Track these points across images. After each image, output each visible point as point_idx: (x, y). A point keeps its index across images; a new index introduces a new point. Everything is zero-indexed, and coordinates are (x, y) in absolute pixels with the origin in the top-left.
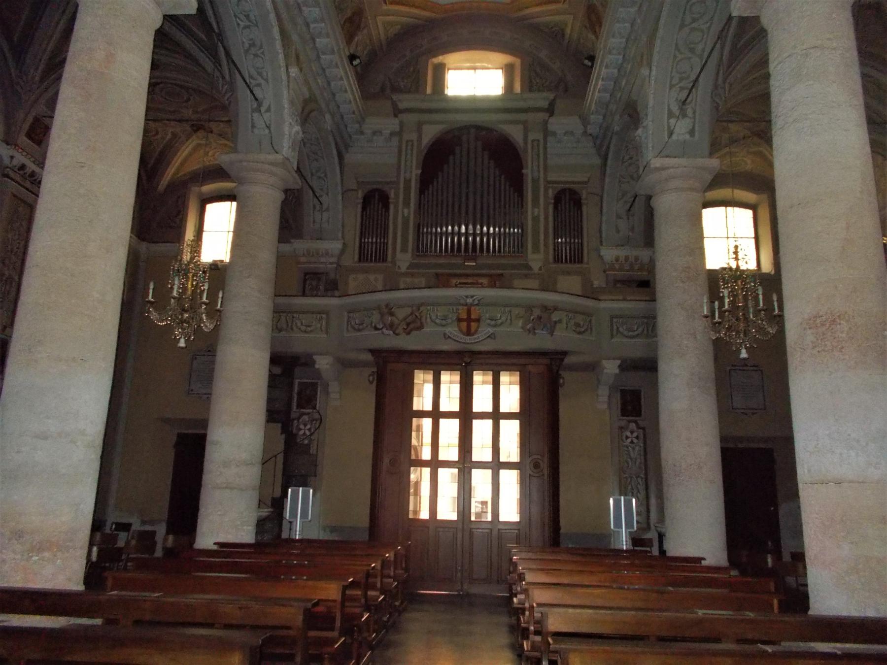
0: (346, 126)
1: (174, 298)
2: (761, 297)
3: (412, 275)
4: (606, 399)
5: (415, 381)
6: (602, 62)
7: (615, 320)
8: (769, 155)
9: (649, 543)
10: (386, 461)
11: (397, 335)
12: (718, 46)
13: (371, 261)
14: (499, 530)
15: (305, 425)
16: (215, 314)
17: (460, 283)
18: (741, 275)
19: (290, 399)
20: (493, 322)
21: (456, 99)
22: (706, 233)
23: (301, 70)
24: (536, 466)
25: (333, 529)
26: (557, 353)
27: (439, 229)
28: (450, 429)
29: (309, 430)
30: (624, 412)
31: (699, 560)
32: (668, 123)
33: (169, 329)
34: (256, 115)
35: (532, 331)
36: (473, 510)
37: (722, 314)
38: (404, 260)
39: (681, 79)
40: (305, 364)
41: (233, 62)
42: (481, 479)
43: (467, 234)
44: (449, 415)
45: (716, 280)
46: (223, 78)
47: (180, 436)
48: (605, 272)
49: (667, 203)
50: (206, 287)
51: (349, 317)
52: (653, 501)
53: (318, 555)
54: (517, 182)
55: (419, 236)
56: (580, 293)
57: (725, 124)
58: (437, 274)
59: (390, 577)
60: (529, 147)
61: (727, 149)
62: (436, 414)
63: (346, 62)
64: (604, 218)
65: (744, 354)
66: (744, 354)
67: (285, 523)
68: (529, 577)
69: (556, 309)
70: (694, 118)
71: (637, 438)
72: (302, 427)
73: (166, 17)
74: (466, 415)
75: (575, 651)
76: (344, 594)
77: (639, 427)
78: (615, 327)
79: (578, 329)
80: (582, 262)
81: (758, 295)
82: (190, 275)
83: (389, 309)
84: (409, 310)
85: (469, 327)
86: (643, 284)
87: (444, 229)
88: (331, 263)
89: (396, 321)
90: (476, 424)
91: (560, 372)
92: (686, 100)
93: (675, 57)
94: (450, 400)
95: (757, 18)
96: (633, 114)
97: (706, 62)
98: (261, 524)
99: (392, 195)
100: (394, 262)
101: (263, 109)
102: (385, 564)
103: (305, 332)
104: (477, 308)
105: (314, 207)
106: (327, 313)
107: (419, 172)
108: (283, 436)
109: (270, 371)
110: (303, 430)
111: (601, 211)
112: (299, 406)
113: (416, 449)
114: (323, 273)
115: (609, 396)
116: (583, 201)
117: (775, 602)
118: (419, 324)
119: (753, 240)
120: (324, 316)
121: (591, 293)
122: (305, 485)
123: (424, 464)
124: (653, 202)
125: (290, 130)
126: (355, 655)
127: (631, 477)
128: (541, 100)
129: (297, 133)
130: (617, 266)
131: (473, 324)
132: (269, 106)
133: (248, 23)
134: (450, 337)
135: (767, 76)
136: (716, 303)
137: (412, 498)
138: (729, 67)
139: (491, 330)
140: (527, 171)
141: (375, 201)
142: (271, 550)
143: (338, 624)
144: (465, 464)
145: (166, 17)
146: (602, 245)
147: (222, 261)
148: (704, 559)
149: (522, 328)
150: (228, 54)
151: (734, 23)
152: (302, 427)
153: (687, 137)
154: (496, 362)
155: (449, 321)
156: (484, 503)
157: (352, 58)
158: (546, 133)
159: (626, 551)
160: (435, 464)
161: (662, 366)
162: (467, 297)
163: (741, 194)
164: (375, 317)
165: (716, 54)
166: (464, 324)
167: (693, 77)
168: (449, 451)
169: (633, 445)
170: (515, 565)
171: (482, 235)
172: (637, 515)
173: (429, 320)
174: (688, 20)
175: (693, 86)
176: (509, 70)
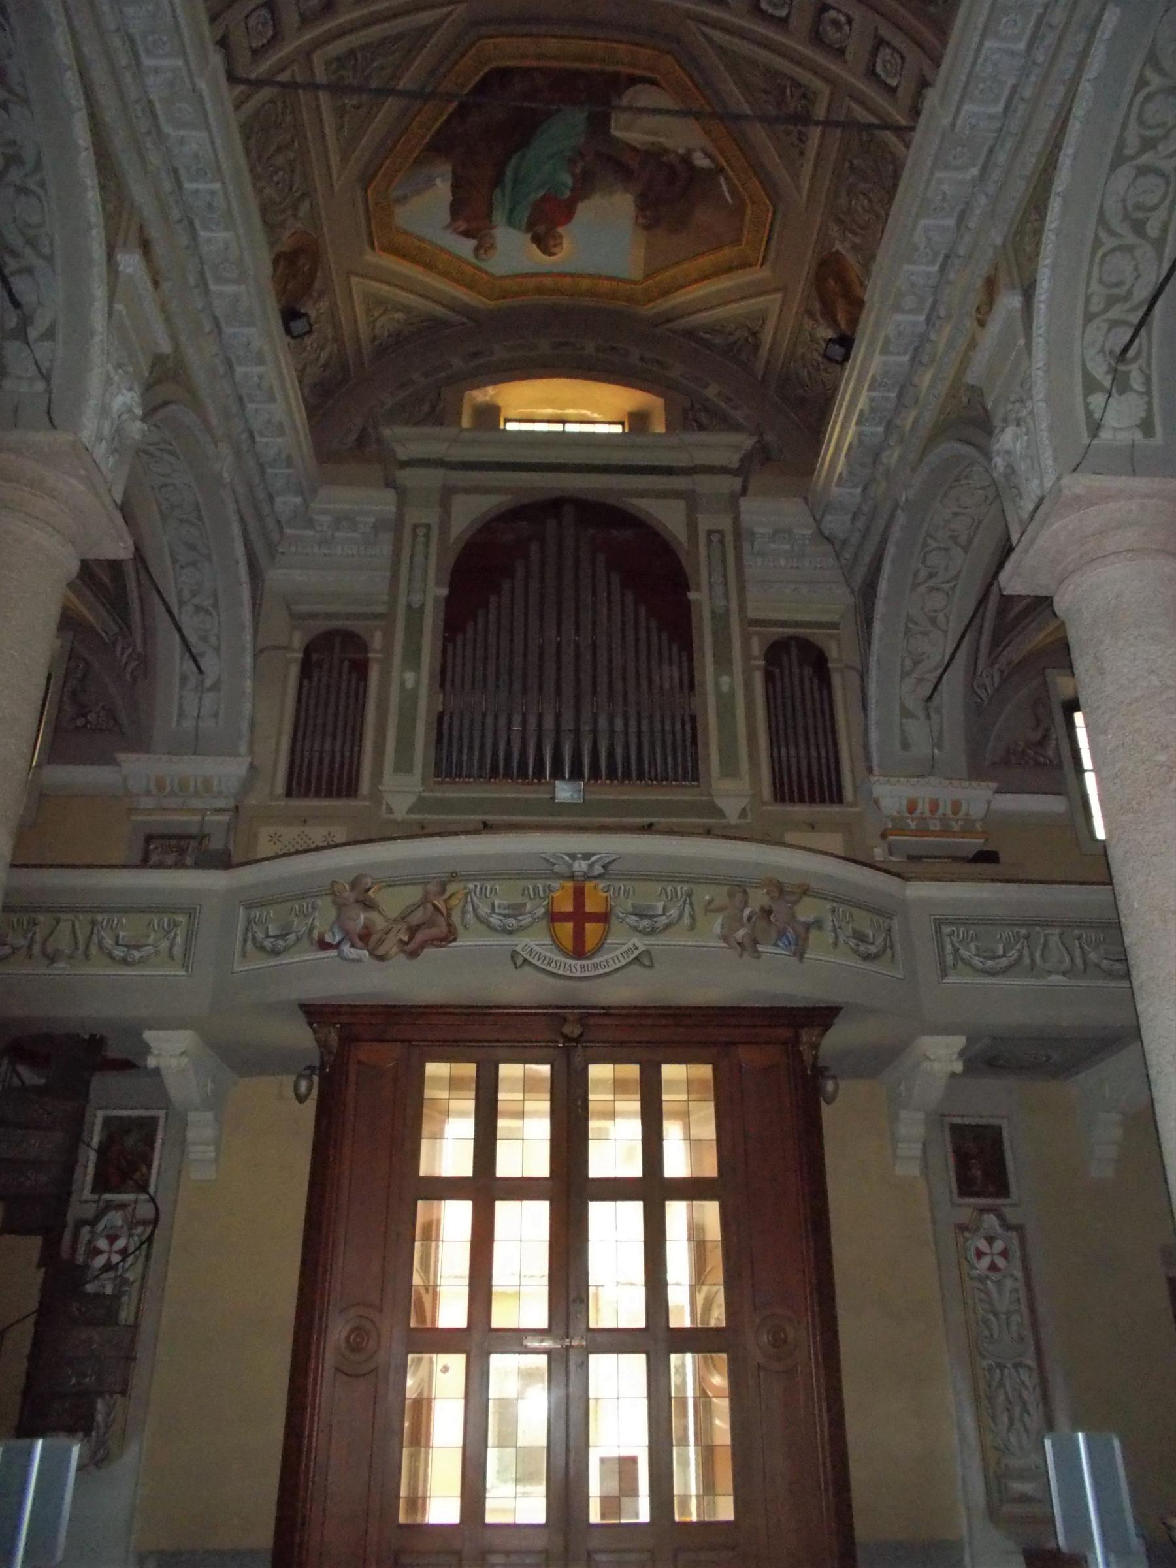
0: (271, 498)
4: (916, 1150)
10: (337, 1331)
11: (381, 958)
15: (112, 1239)
20: (645, 922)
28: (524, 1227)
30: (966, 1187)
32: (1087, 405)
35: (749, 947)
39: (1111, 301)
40: (126, 1065)
62: (485, 1188)
69: (805, 891)
70: (1148, 393)
71: (1004, 1254)
72: (102, 1244)
77: (1006, 1226)
78: (949, 948)
80: (840, 801)
89: (380, 923)
90: (600, 1213)
93: (1097, 242)
94: (526, 1149)
99: (377, 641)
100: (376, 797)
101: (33, 334)
103: (125, 962)
104: (602, 885)
105: (184, 679)
106: (191, 913)
107: (444, 592)
112: (102, 1183)
114: (191, 837)
118: (441, 929)
120: (182, 919)
123: (448, 1341)
127: (1002, 1367)
130: (913, 825)
131: (589, 926)
139: (641, 943)
141: (333, 664)
149: (725, 938)
152: (102, 1244)
153: (1138, 435)
154: (651, 1035)
155: (527, 920)
156: (627, 1464)
160: (480, 1340)
162: (573, 856)
164: (323, 919)
167: (1142, 293)
168: (523, 1299)
169: (995, 1276)
173: (470, 916)
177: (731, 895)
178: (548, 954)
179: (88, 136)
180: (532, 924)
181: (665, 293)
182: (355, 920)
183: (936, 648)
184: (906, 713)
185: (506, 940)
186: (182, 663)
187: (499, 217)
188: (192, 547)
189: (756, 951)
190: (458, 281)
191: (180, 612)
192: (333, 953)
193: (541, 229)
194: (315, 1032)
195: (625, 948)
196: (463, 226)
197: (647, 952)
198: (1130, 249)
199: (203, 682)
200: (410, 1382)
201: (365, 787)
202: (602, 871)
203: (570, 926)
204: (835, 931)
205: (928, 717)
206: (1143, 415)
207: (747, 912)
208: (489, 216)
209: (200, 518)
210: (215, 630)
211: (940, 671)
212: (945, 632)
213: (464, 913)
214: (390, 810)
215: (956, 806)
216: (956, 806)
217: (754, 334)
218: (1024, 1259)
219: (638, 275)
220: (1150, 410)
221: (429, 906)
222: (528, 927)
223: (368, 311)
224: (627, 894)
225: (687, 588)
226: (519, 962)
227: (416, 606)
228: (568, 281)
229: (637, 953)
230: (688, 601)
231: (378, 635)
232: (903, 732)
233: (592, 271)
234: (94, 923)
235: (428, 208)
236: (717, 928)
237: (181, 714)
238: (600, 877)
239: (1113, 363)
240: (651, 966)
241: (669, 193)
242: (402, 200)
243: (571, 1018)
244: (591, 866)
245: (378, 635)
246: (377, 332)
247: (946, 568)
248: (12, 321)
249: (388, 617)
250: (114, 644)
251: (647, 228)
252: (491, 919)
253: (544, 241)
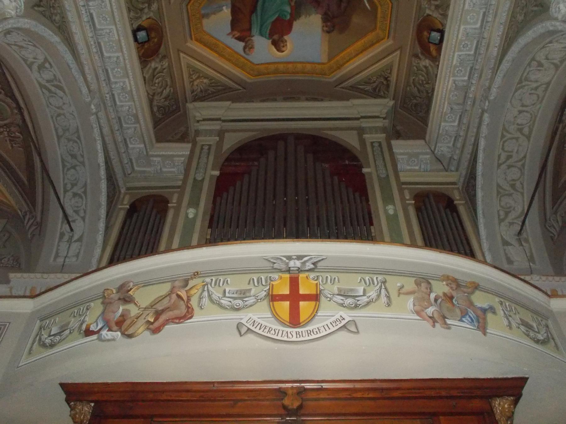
11: (130, 336)
20: (349, 301)
84: (165, 289)
89: (133, 310)
104: (312, 275)
105: (62, 235)
118: (183, 310)
139: (347, 315)
149: (418, 313)
155: (251, 300)
162: (289, 258)
164: (93, 317)
177: (418, 284)
178: (269, 325)
180: (255, 303)
181: (339, 67)
182: (114, 312)
183: (519, 204)
184: (506, 243)
186: (62, 226)
187: (255, 30)
188: (74, 156)
189: (445, 323)
190: (236, 65)
191: (64, 197)
192: (95, 337)
193: (276, 37)
194: (72, 409)
195: (334, 319)
196: (238, 34)
199: (72, 237)
202: (312, 266)
203: (287, 304)
207: (433, 296)
208: (250, 29)
209: (79, 138)
210: (84, 206)
211: (522, 218)
212: (522, 194)
213: (200, 298)
217: (386, 79)
219: (325, 60)
221: (174, 296)
222: (251, 306)
223: (190, 75)
224: (333, 281)
225: (361, 167)
226: (244, 330)
227: (200, 179)
228: (290, 66)
229: (344, 322)
230: (363, 175)
231: (176, 196)
232: (506, 254)
233: (301, 60)
237: (57, 256)
238: (310, 270)
240: (358, 332)
242: (206, 16)
243: (290, 392)
244: (304, 263)
245: (176, 196)
246: (195, 88)
247: (517, 152)
249: (182, 188)
250: (24, 217)
251: (328, 32)
252: (222, 301)
253: (278, 44)
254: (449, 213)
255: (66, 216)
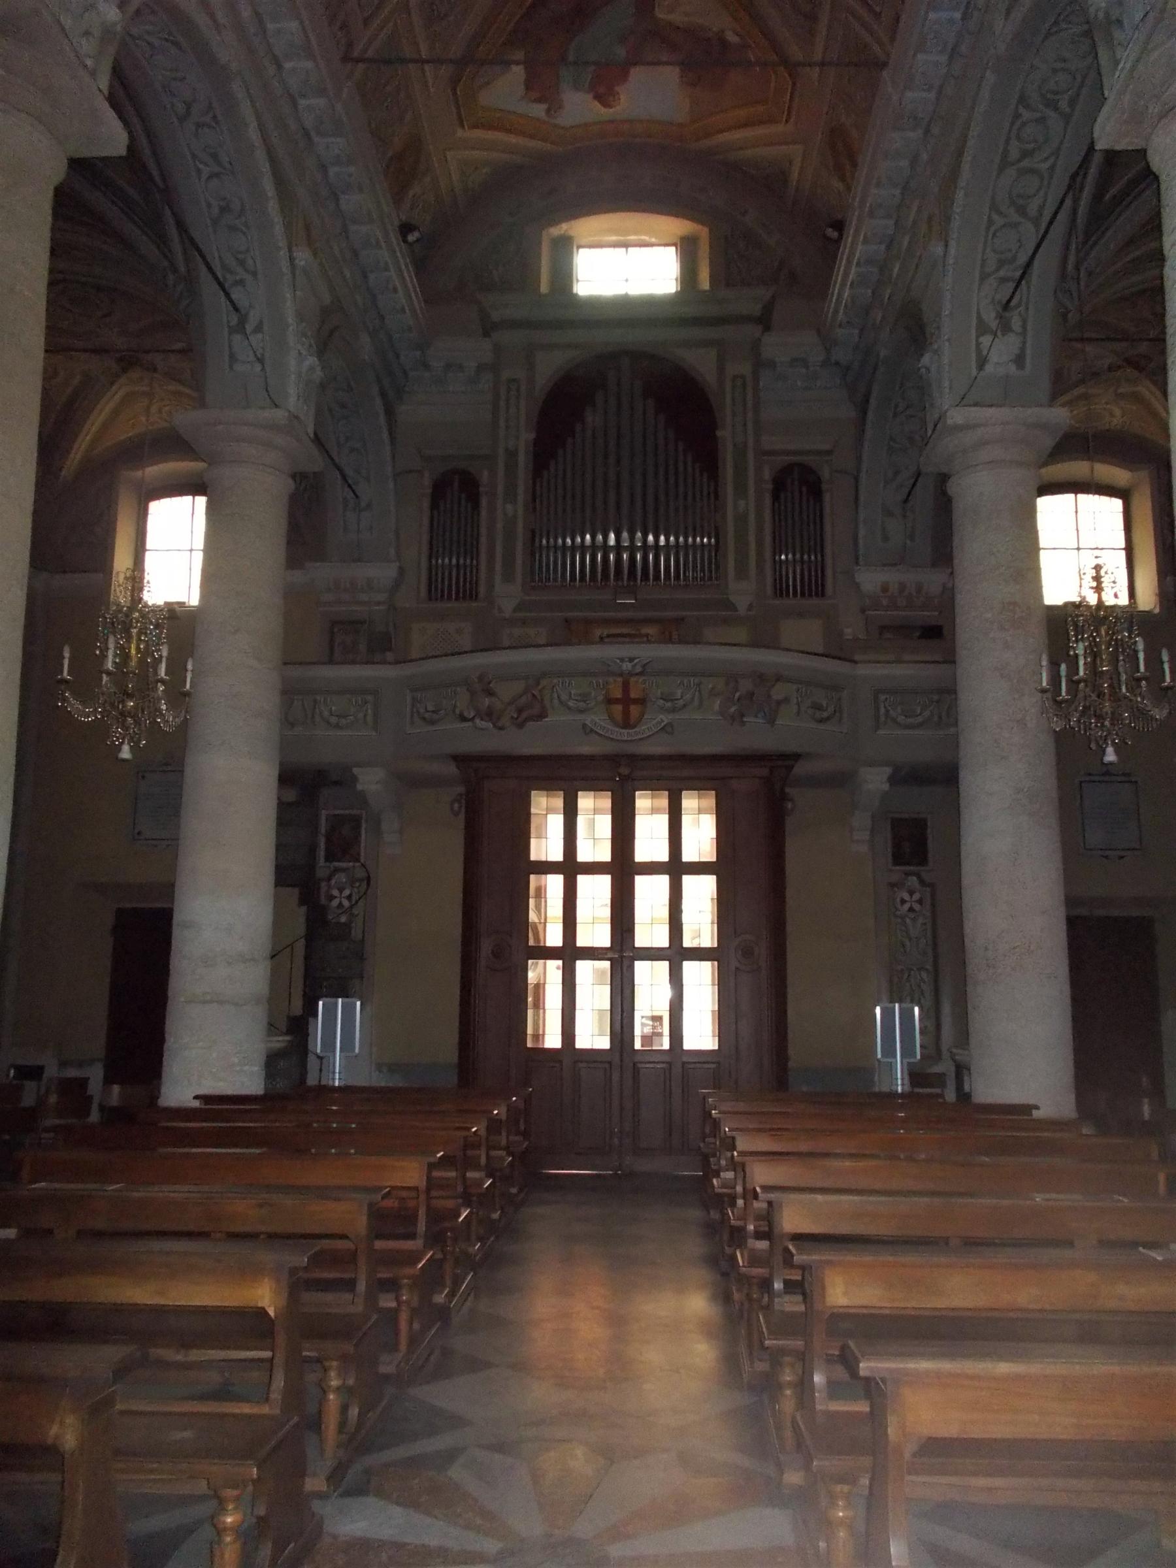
0: (398, 356)
1: (109, 673)
2: (1141, 656)
3: (524, 622)
5: (533, 810)
6: (857, 231)
7: (882, 697)
8: (1161, 410)
9: (940, 1079)
10: (486, 947)
11: (501, 728)
12: (1068, 202)
13: (449, 597)
14: (684, 1063)
15: (341, 890)
16: (179, 697)
17: (608, 636)
18: (1105, 618)
19: (313, 849)
20: (669, 704)
21: (595, 303)
22: (1043, 541)
23: (315, 254)
24: (747, 952)
25: (393, 1068)
26: (783, 756)
27: (569, 541)
28: (595, 892)
29: (349, 897)
30: (898, 858)
31: (1027, 1109)
32: (978, 344)
33: (100, 730)
34: (237, 338)
36: (638, 1032)
37: (1073, 684)
38: (507, 596)
41: (192, 240)
42: (651, 980)
43: (618, 548)
44: (593, 868)
45: (1066, 623)
46: (175, 270)
47: (120, 912)
48: (863, 611)
49: (978, 488)
50: (165, 654)
51: (413, 699)
52: (946, 1009)
53: (378, 1113)
54: (706, 454)
55: (533, 554)
56: (821, 650)
57: (1079, 345)
58: (567, 621)
59: (500, 1149)
60: (728, 388)
61: (1081, 390)
62: (571, 868)
63: (394, 238)
64: (862, 516)
65: (1110, 756)
66: (1110, 756)
67: (311, 1059)
68: (742, 1144)
69: (779, 678)
70: (1024, 333)
71: (920, 902)
73: (77, 165)
74: (623, 868)
75: (830, 1263)
76: (429, 1178)
77: (922, 882)
78: (882, 710)
79: (818, 714)
80: (823, 595)
81: (1136, 652)
82: (134, 631)
83: (483, 685)
85: (626, 713)
86: (934, 633)
87: (579, 540)
88: (379, 603)
91: (787, 790)
92: (1009, 301)
93: (990, 222)
94: (595, 844)
95: (1142, 153)
96: (916, 331)
97: (1046, 232)
98: (272, 1062)
99: (485, 477)
101: (249, 328)
102: (494, 1126)
103: (338, 726)
107: (533, 436)
108: (304, 909)
109: (279, 798)
110: (338, 896)
111: (857, 499)
112: (330, 857)
113: (535, 926)
115: (872, 831)
116: (824, 487)
117: (1162, 1178)
119: (1123, 553)
120: (370, 698)
121: (839, 651)
122: (345, 994)
124: (953, 488)
125: (299, 366)
126: (448, 1282)
128: (748, 301)
129: (311, 369)
130: (885, 602)
131: (632, 707)
132: (261, 322)
133: (217, 169)
134: (597, 732)
135: (1159, 258)
136: (1063, 667)
137: (530, 1013)
138: (1085, 243)
139: (665, 718)
140: (724, 433)
141: (455, 492)
142: (289, 1108)
143: (421, 1227)
144: (622, 953)
145: (77, 165)
146: (857, 563)
147: (181, 604)
148: (1037, 1108)
150: (181, 226)
151: (1097, 159)
152: (335, 892)
153: (1013, 368)
154: (674, 775)
156: (657, 1019)
157: (406, 229)
158: (759, 364)
159: (902, 1095)
160: (570, 953)
161: (965, 776)
162: (622, 660)
163: (1107, 472)
165: (1062, 217)
166: (618, 709)
167: (1023, 259)
168: (595, 930)
169: (912, 915)
170: (716, 1124)
171: (645, 547)
172: (921, 1033)
173: (556, 701)
174: (1014, 154)
175: (1024, 273)
176: (687, 249)
179: (267, 165)
185: (579, 717)
188: (343, 406)
192: (470, 724)
197: (670, 724)
198: (1015, 225)
200: (530, 975)
201: (482, 590)
204: (798, 704)
205: (904, 516)
206: (1017, 351)
207: (737, 695)
213: (552, 700)
214: (500, 610)
215: (919, 589)
216: (919, 589)
218: (933, 905)
220: (1023, 349)
221: (529, 695)
231: (486, 473)
234: (315, 701)
235: (506, 89)
236: (717, 707)
239: (1000, 310)
241: (703, 59)
245: (486, 473)
248: (234, 320)
253: (604, 97)
254: (812, 502)
255: (344, 477)
